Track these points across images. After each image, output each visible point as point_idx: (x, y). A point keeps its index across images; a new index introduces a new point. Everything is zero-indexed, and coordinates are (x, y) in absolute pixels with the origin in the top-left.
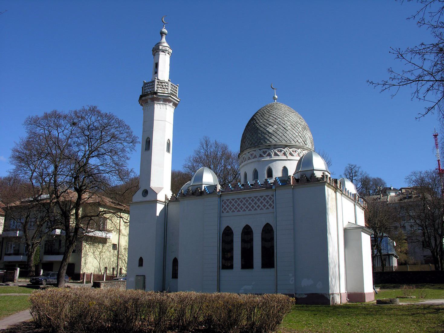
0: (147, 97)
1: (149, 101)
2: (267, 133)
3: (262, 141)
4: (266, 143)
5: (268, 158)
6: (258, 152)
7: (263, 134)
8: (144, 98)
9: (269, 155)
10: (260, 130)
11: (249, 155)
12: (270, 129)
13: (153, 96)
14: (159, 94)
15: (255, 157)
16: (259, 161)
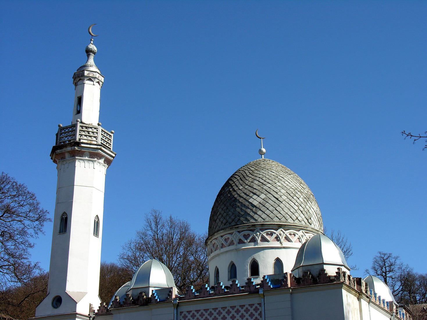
0: (64, 149)
1: (67, 155)
2: (250, 207)
3: (242, 219)
4: (249, 222)
5: (252, 246)
6: (236, 236)
7: (243, 208)
8: (59, 151)
9: (254, 240)
10: (240, 202)
11: (222, 240)
12: (255, 201)
13: (73, 148)
14: (83, 145)
15: (232, 243)
16: (237, 250)
